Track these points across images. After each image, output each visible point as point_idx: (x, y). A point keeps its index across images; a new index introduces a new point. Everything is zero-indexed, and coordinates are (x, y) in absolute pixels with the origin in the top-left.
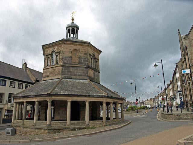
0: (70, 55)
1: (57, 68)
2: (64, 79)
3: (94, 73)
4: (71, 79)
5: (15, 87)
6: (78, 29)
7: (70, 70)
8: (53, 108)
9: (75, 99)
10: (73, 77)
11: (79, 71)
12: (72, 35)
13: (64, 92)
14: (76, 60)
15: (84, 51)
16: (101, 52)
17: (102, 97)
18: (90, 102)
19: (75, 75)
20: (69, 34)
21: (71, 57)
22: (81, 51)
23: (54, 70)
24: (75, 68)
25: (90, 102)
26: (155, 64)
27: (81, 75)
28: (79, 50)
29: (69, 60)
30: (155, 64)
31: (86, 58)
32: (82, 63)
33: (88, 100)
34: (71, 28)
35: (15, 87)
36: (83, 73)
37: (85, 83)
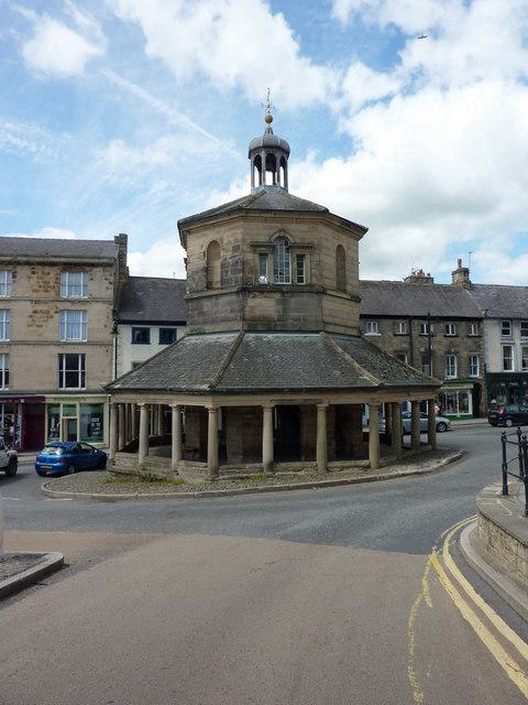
4: (205, 333)
6: (288, 153)
10: (208, 328)
12: (269, 176)
15: (232, 239)
16: (364, 230)
17: (202, 393)
18: (329, 410)
19: (214, 322)
20: (260, 170)
24: (214, 300)
25: (148, 406)
27: (225, 320)
28: (222, 240)
32: (229, 281)
34: (263, 155)
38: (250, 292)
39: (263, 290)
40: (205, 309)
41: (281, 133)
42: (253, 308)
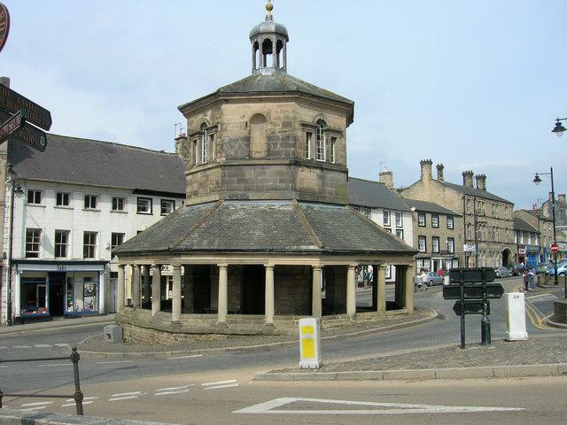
0: (244, 133)
1: (212, 171)
2: (226, 203)
3: (322, 178)
5: (151, 214)
7: (243, 175)
8: (419, 263)
9: (236, 260)
10: (251, 195)
11: (271, 175)
13: (211, 243)
14: (259, 145)
15: (282, 115)
17: (310, 254)
18: (231, 270)
19: (259, 190)
21: (248, 139)
22: (273, 116)
23: (207, 176)
24: (258, 169)
26: (558, 124)
28: (269, 113)
29: (240, 146)
30: (558, 124)
31: (288, 137)
32: (277, 153)
33: (270, 263)
35: (151, 214)
36: (281, 181)
37: (283, 212)
38: (300, 166)
39: (310, 165)
40: (248, 176)
41: (280, 19)
42: (302, 180)
